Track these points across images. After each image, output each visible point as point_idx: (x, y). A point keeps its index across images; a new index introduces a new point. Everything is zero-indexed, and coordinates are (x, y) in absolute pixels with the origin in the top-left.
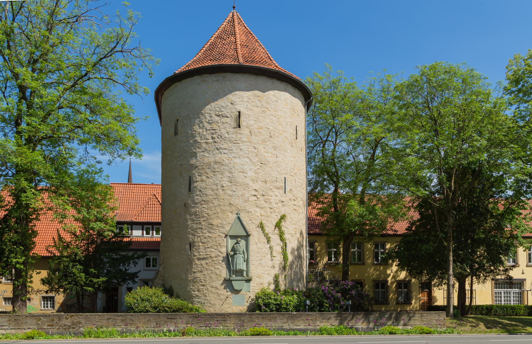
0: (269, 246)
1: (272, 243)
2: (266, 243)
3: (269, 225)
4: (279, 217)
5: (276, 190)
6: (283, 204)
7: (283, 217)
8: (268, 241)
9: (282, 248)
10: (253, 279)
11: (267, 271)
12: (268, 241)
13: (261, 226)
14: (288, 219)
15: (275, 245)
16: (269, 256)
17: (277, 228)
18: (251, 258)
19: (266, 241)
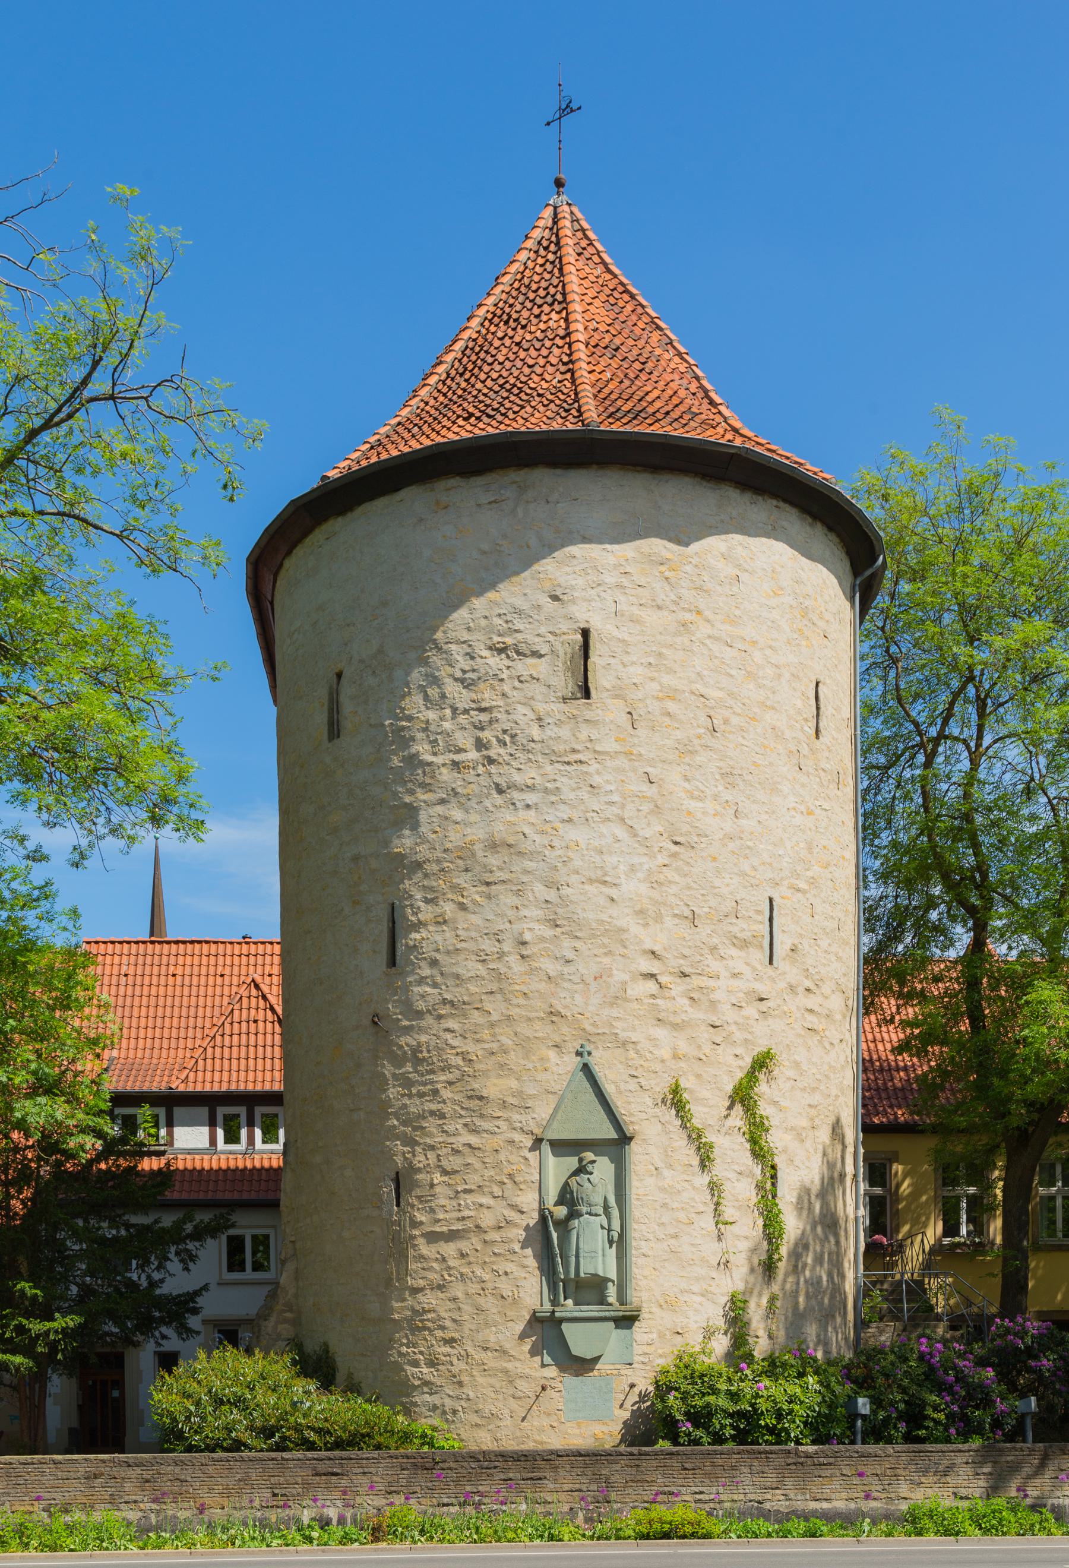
0: (706, 1179)
6: (763, 1006)
7: (761, 1064)
8: (705, 1162)
9: (760, 1187)
10: (644, 1315)
12: (705, 1162)
14: (783, 1070)
15: (732, 1175)
16: (708, 1222)
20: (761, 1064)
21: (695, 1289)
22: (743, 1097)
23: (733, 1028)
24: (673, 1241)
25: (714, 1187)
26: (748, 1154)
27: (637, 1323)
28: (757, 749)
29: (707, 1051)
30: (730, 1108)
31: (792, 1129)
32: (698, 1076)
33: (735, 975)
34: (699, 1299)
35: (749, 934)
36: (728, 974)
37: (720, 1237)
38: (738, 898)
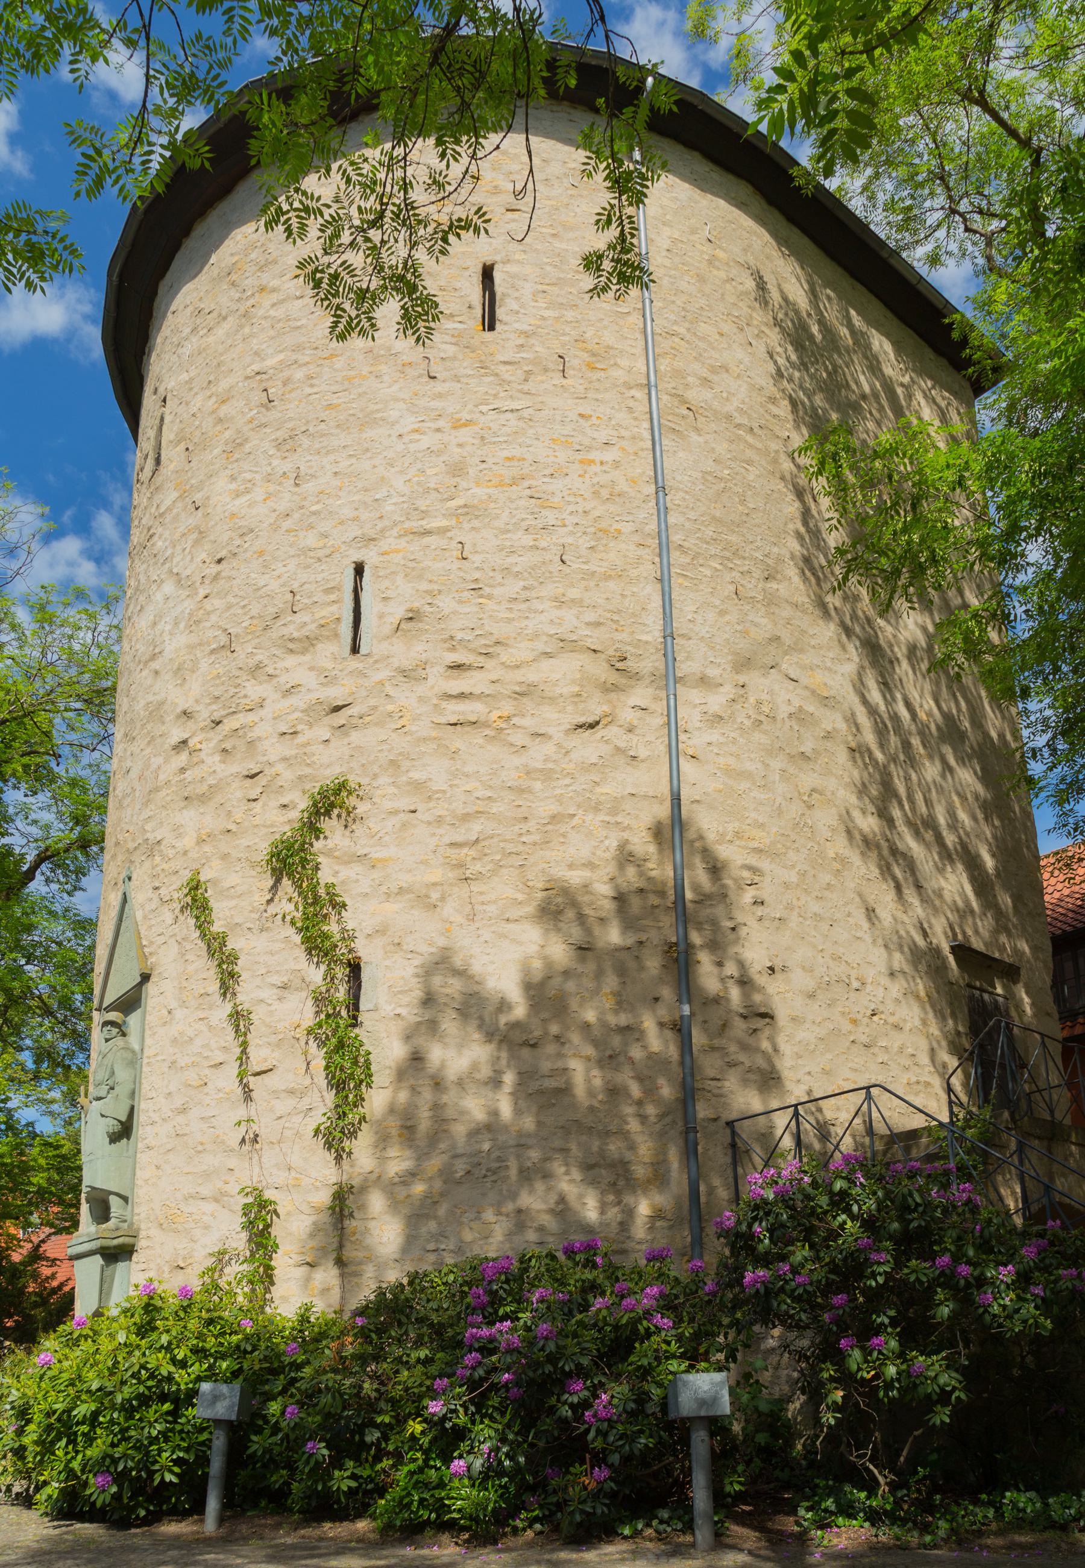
0: (228, 1008)
1: (247, 993)
2: (217, 997)
3: (233, 879)
4: (304, 803)
5: (291, 661)
6: (341, 718)
7: (330, 803)
8: (228, 980)
9: (321, 1000)
10: (141, 1244)
11: (207, 1175)
12: (228, 980)
13: (196, 902)
14: (380, 802)
15: (267, 994)
16: (227, 1080)
17: (286, 882)
18: (944, 1097)
19: (214, 987)
20: (330, 803)
21: (205, 1191)
22: (290, 861)
23: (280, 768)
24: (181, 1119)
25: (239, 1019)
26: (301, 953)
27: (135, 1255)
28: (334, 388)
29: (238, 816)
30: (274, 888)
31: (401, 891)
32: (225, 857)
33: (289, 692)
34: (209, 1207)
35: (313, 626)
36: (278, 696)
37: (248, 1094)
38: (295, 586)
